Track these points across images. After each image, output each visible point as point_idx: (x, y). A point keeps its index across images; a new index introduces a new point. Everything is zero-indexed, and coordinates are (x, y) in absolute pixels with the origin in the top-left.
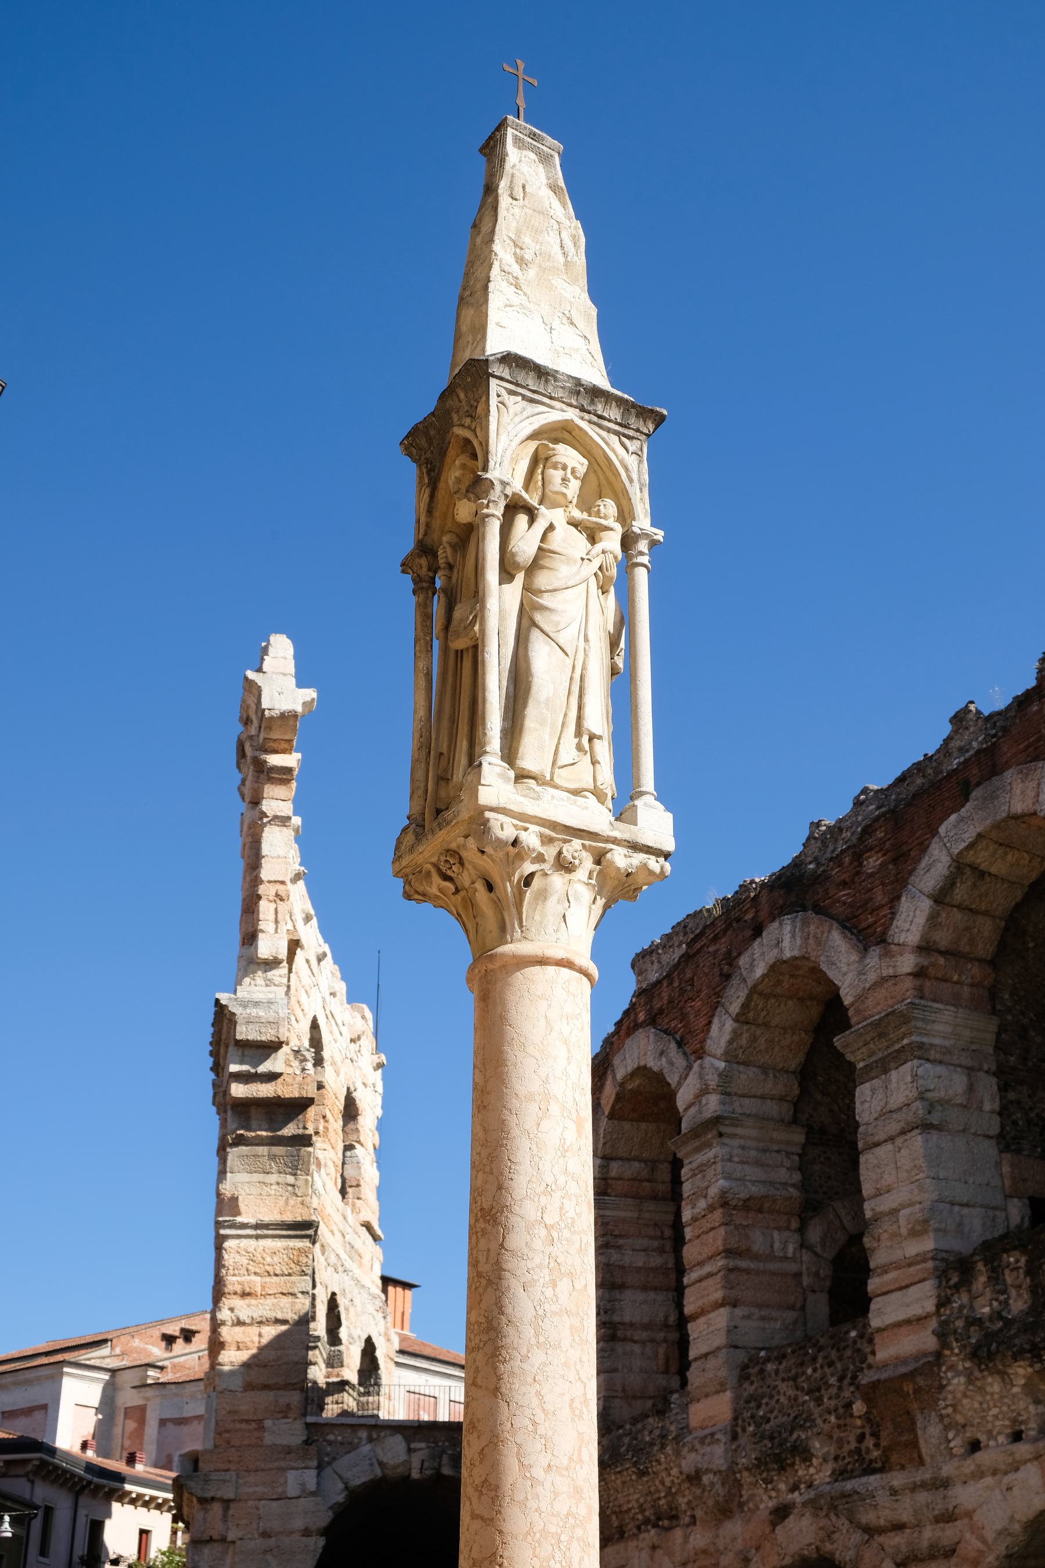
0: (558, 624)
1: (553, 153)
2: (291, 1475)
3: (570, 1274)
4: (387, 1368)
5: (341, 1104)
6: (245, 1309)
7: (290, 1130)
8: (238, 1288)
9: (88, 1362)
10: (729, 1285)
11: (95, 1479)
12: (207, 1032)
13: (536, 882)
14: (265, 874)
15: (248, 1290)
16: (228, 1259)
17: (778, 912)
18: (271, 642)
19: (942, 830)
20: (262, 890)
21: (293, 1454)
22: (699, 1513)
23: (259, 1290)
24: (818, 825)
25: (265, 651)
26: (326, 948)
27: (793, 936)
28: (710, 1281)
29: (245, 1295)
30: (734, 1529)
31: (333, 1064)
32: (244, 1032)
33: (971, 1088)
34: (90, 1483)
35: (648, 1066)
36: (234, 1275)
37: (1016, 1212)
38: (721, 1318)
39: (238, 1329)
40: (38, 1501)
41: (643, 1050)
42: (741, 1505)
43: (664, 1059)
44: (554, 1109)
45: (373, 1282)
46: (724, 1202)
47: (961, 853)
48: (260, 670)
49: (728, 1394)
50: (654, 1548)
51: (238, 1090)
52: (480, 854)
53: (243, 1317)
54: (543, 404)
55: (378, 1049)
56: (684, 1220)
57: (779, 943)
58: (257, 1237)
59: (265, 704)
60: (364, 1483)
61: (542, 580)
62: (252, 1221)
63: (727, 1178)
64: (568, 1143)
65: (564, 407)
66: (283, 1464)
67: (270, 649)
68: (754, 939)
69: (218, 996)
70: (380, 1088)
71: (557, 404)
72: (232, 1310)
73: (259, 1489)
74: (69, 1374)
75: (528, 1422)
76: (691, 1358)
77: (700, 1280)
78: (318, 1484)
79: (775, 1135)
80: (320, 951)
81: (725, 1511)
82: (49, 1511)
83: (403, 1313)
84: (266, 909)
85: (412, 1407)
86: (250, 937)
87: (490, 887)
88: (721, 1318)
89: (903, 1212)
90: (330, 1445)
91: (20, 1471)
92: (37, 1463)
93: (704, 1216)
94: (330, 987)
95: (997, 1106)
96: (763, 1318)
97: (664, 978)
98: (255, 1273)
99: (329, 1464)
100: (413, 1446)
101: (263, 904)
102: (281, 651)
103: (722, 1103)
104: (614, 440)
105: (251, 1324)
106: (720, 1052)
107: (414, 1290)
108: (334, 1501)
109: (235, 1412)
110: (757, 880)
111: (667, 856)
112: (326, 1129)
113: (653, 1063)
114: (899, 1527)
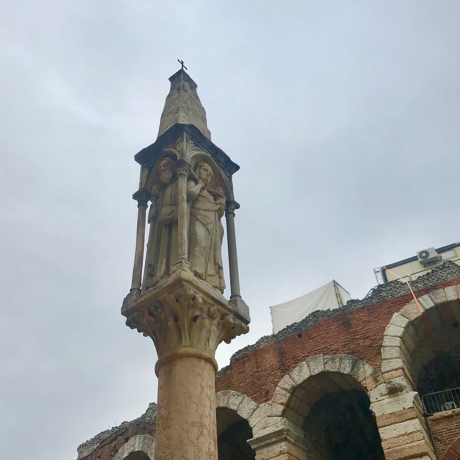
0: (207, 221)
13: (198, 321)
27: (139, 443)
52: (176, 302)
54: (201, 148)
64: (212, 451)
87: (176, 319)
97: (89, 455)
104: (222, 170)
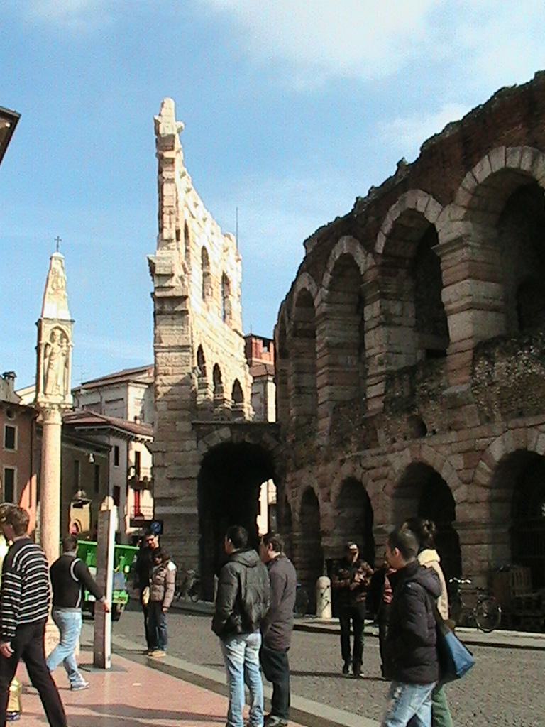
2: (187, 443)
5: (220, 280)
6: (166, 380)
7: (179, 308)
8: (163, 372)
10: (329, 378)
15: (166, 372)
19: (390, 210)
20: (164, 210)
23: (170, 372)
28: (323, 376)
29: (165, 375)
30: (331, 466)
31: (215, 263)
33: (403, 309)
37: (420, 355)
38: (327, 390)
39: (164, 388)
40: (111, 444)
41: (305, 282)
42: (333, 458)
46: (328, 345)
47: (396, 220)
48: (160, 115)
49: (329, 419)
51: (158, 294)
53: (165, 383)
57: (342, 246)
58: (169, 352)
61: (52, 358)
62: (167, 345)
63: (329, 336)
69: (148, 256)
72: (161, 380)
79: (349, 318)
81: (327, 460)
82: (117, 448)
84: (166, 217)
88: (327, 390)
89: (377, 356)
91: (104, 432)
95: (414, 314)
96: (343, 389)
101: (165, 216)
102: (170, 103)
103: (327, 306)
112: (212, 293)
114: (373, 468)
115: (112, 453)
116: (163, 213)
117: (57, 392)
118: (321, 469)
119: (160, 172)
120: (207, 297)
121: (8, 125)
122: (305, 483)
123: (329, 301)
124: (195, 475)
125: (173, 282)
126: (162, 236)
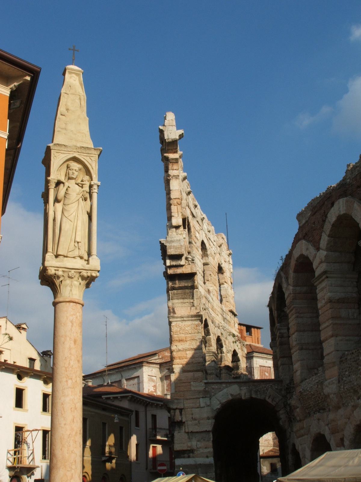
1: (80, 73)
3: (71, 379)
4: (243, 360)
8: (177, 339)
9: (151, 361)
11: (151, 401)
12: (159, 252)
14: (172, 196)
16: (174, 329)
17: (341, 196)
18: (167, 115)
21: (201, 393)
22: (331, 407)
24: (348, 166)
25: (165, 118)
26: (204, 216)
32: (171, 251)
34: (149, 402)
35: (303, 254)
36: (176, 334)
43: (308, 251)
44: (68, 339)
45: (236, 331)
46: (330, 301)
48: (164, 125)
50: (319, 419)
51: (170, 272)
55: (228, 249)
56: (318, 307)
59: (166, 137)
60: (226, 401)
65: (73, 153)
66: (198, 397)
67: (167, 117)
68: (332, 208)
70: (231, 262)
71: (71, 153)
73: (191, 405)
74: (145, 366)
75: (60, 414)
76: (324, 355)
77: (325, 328)
78: (210, 402)
80: (202, 217)
82: (137, 413)
83: (258, 338)
84: (174, 208)
85: (262, 371)
86: (170, 218)
88: (332, 341)
90: (213, 389)
92: (130, 397)
93: (324, 306)
94: (208, 229)
98: (183, 333)
99: (214, 395)
100: (241, 388)
101: (172, 207)
102: (171, 117)
105: (183, 351)
106: (324, 248)
107: (261, 329)
108: (217, 408)
109: (181, 380)
110: (332, 186)
111: (98, 271)
113: (305, 253)
115: (133, 416)
116: (171, 205)
117: (76, 253)
118: (331, 416)
119: (167, 170)
120: (207, 283)
121: (28, 78)
122: (314, 430)
123: (327, 260)
124: (210, 428)
125: (183, 262)
126: (171, 224)
